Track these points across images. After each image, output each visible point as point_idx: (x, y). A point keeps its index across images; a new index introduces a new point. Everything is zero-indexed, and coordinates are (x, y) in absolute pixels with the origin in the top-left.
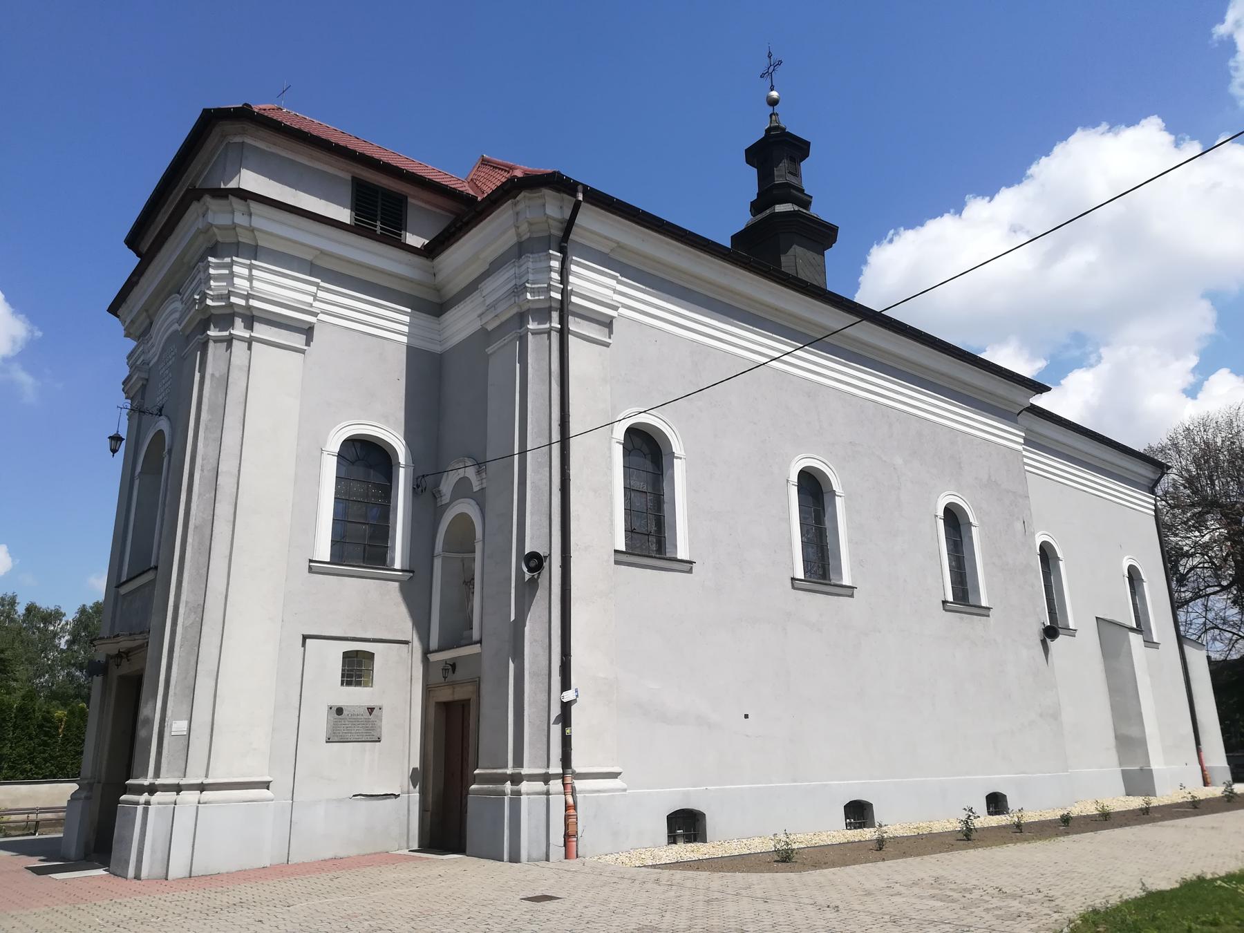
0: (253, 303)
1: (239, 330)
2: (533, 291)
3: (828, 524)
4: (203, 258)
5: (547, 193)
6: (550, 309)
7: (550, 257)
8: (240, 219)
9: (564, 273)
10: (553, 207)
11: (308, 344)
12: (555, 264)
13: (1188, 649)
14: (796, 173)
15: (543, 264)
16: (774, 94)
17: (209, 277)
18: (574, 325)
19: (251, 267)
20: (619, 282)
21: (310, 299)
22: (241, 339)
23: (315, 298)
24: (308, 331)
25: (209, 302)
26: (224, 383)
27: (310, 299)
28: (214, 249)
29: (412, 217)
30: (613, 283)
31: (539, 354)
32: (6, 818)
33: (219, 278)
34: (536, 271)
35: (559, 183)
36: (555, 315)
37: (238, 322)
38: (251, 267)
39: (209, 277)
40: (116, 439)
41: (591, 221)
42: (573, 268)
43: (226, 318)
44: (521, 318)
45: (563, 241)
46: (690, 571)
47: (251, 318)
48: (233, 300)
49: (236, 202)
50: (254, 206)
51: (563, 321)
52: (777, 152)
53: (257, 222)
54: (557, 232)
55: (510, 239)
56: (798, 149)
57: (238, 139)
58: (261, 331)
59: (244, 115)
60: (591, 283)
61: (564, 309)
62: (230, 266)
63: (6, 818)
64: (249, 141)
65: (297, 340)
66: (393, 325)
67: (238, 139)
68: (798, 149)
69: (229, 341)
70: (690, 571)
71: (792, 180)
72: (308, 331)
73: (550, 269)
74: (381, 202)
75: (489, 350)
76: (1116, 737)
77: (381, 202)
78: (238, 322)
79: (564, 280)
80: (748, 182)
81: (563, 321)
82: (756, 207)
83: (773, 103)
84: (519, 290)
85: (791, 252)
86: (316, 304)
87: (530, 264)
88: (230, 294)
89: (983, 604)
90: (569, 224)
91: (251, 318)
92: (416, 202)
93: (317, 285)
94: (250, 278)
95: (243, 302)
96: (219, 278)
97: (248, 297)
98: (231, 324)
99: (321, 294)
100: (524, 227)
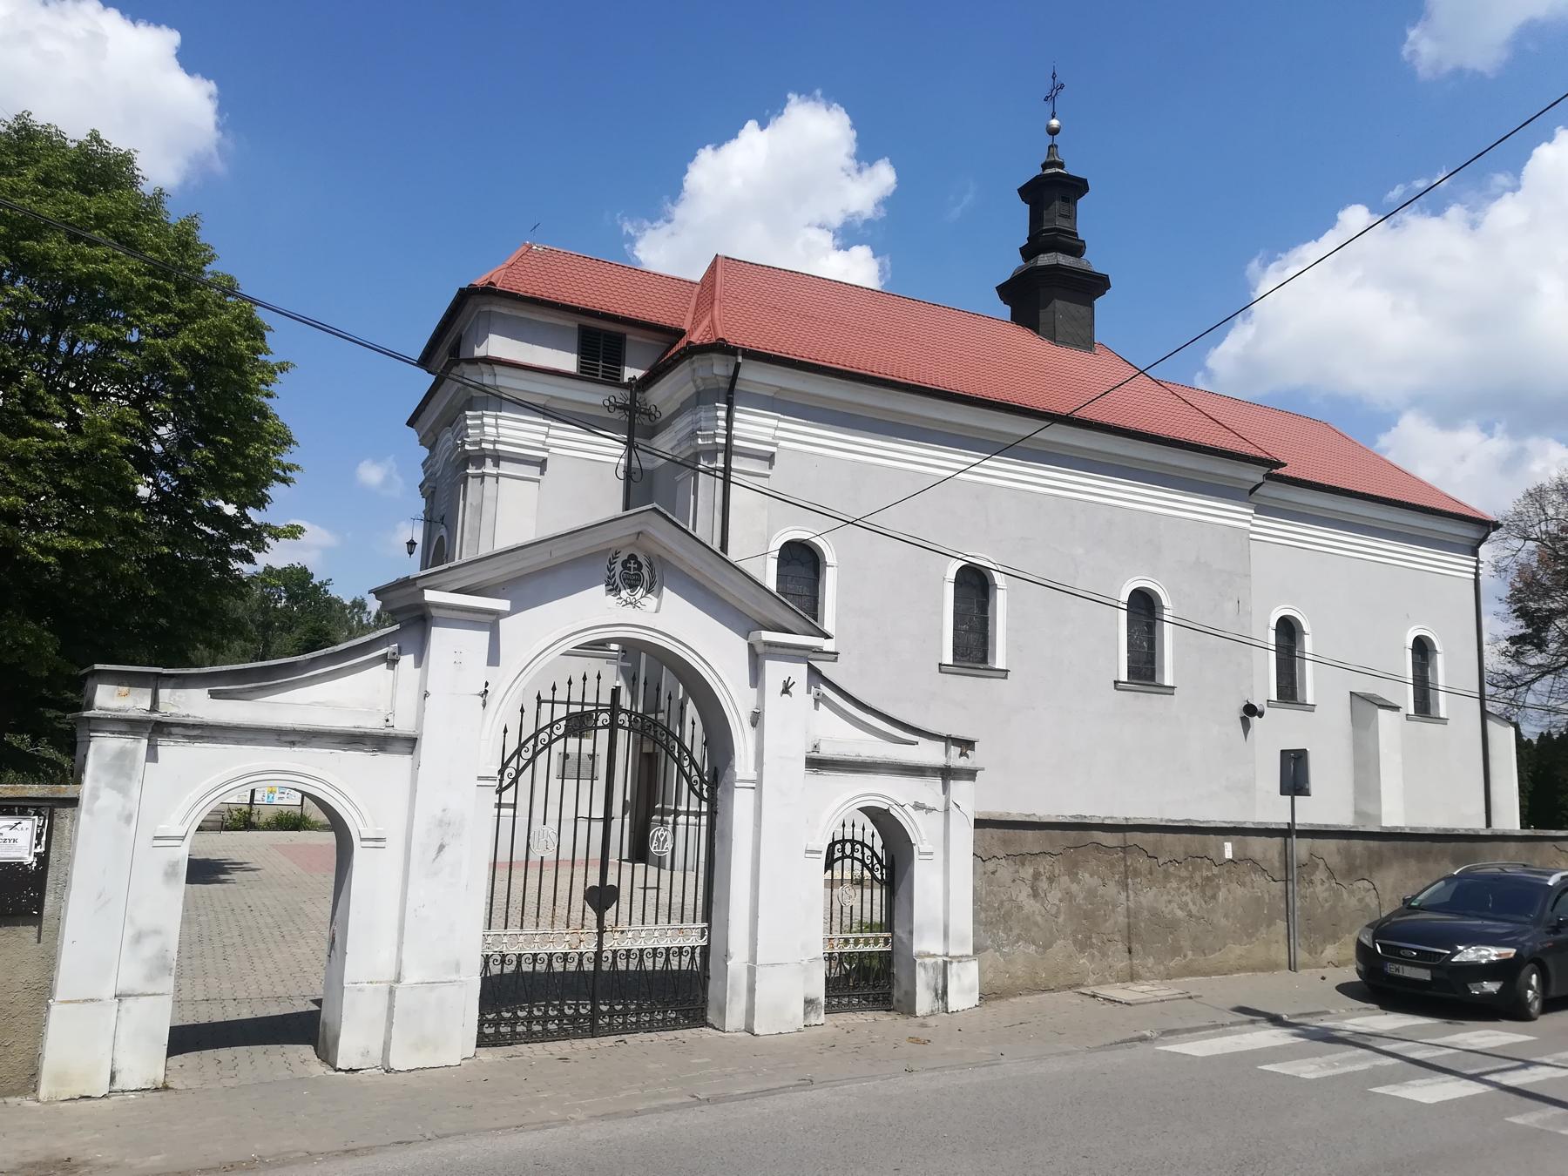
0: (498, 447)
1: (489, 468)
2: (703, 437)
3: (990, 614)
4: (462, 410)
5: (714, 356)
6: (717, 451)
7: (717, 409)
8: (487, 380)
9: (729, 419)
10: (719, 368)
11: (542, 473)
12: (722, 414)
13: (1492, 726)
14: (1071, 216)
15: (711, 414)
16: (1055, 123)
17: (467, 427)
18: (736, 463)
19: (497, 417)
20: (780, 420)
21: (543, 438)
22: (491, 475)
23: (547, 436)
24: (542, 464)
25: (467, 447)
26: (479, 510)
27: (543, 438)
28: (470, 404)
29: (630, 352)
30: (774, 422)
31: (708, 489)
32: (397, 627)
33: (474, 427)
34: (707, 419)
35: (721, 348)
36: (721, 456)
37: (489, 461)
38: (497, 417)
39: (467, 427)
40: (412, 544)
41: (754, 376)
42: (737, 415)
43: (479, 458)
44: (696, 456)
45: (730, 395)
46: (836, 660)
47: (498, 458)
48: (484, 445)
49: (484, 367)
50: (498, 369)
51: (727, 461)
52: (1052, 192)
53: (500, 381)
54: (725, 385)
55: (690, 389)
56: (1076, 187)
57: (486, 308)
58: (506, 468)
59: (488, 292)
60: (752, 426)
61: (729, 450)
62: (481, 417)
63: (397, 627)
64: (495, 309)
65: (533, 472)
66: (609, 451)
67: (486, 308)
68: (1076, 187)
69: (482, 476)
70: (836, 660)
71: (1061, 223)
72: (542, 464)
73: (717, 418)
74: (601, 342)
75: (678, 478)
76: (1356, 813)
77: (601, 342)
78: (489, 461)
79: (729, 428)
80: (1017, 222)
81: (727, 461)
82: (1028, 252)
83: (1054, 132)
84: (693, 435)
85: (1051, 307)
86: (549, 441)
87: (703, 414)
88: (481, 441)
89: (1167, 683)
90: (734, 378)
91: (498, 458)
92: (633, 336)
93: (549, 426)
94: (497, 426)
95: (491, 447)
96: (474, 427)
97: (494, 442)
98: (483, 464)
99: (552, 432)
100: (699, 381)
